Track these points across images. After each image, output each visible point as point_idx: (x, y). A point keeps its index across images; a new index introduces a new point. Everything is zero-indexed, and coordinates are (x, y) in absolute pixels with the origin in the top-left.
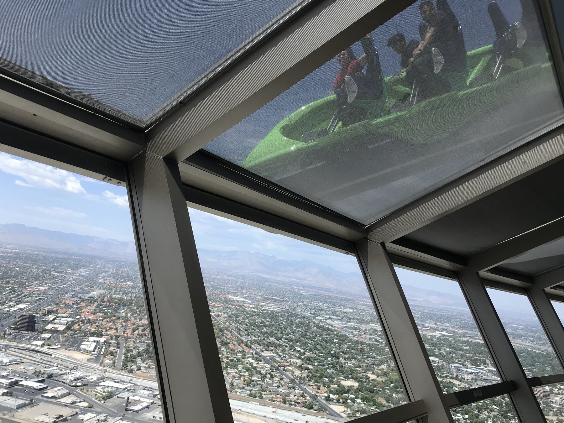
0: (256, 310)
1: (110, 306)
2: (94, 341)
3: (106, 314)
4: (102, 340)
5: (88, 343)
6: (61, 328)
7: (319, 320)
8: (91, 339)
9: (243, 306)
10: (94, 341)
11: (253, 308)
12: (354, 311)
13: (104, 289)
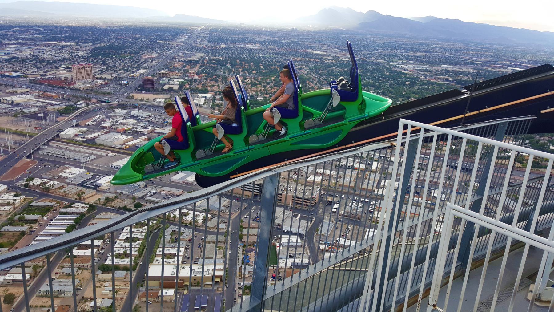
0: (333, 61)
1: (209, 66)
2: (203, 97)
3: (208, 74)
4: (209, 95)
5: (198, 99)
6: (176, 88)
7: (392, 65)
8: (200, 95)
9: (322, 58)
10: (203, 97)
11: (332, 60)
12: (426, 54)
13: (202, 53)
